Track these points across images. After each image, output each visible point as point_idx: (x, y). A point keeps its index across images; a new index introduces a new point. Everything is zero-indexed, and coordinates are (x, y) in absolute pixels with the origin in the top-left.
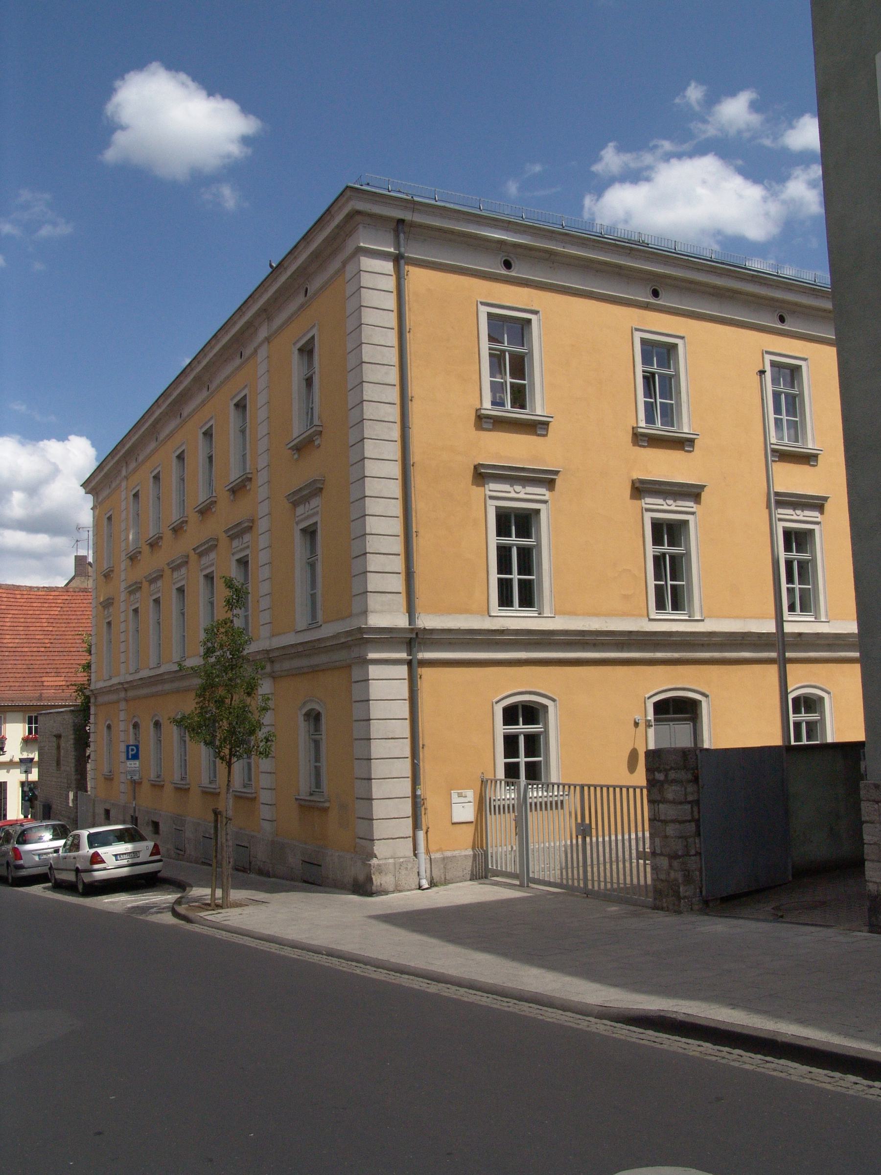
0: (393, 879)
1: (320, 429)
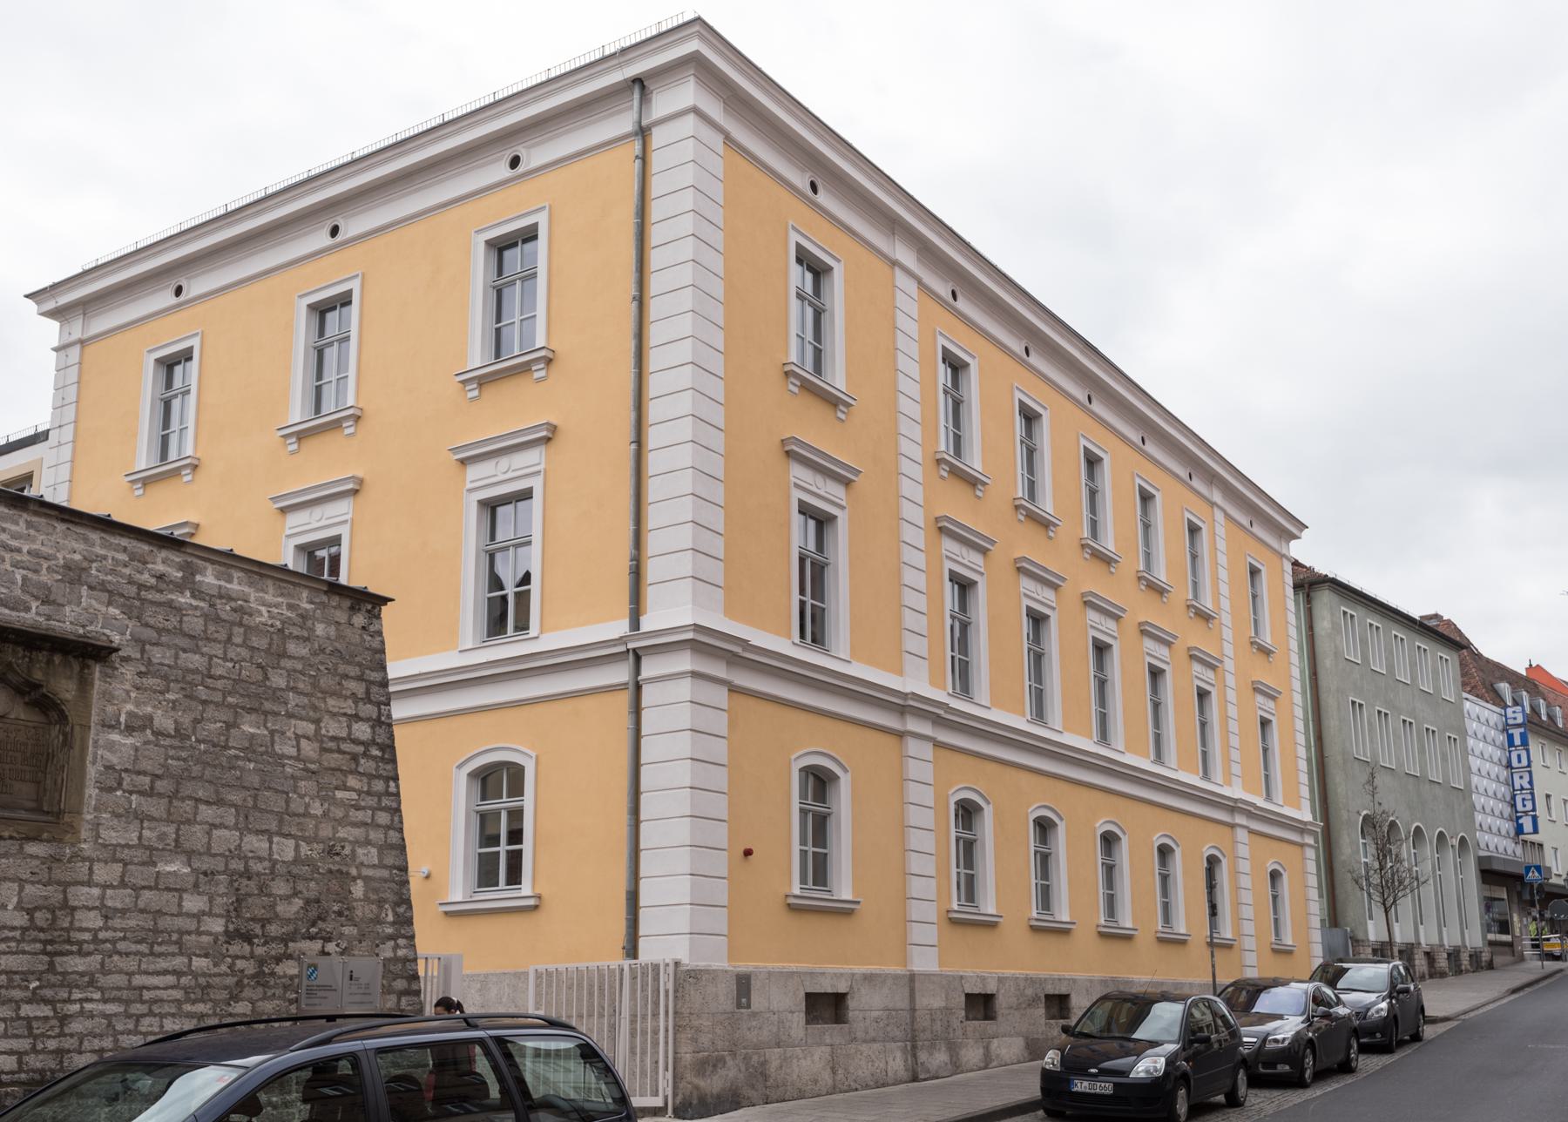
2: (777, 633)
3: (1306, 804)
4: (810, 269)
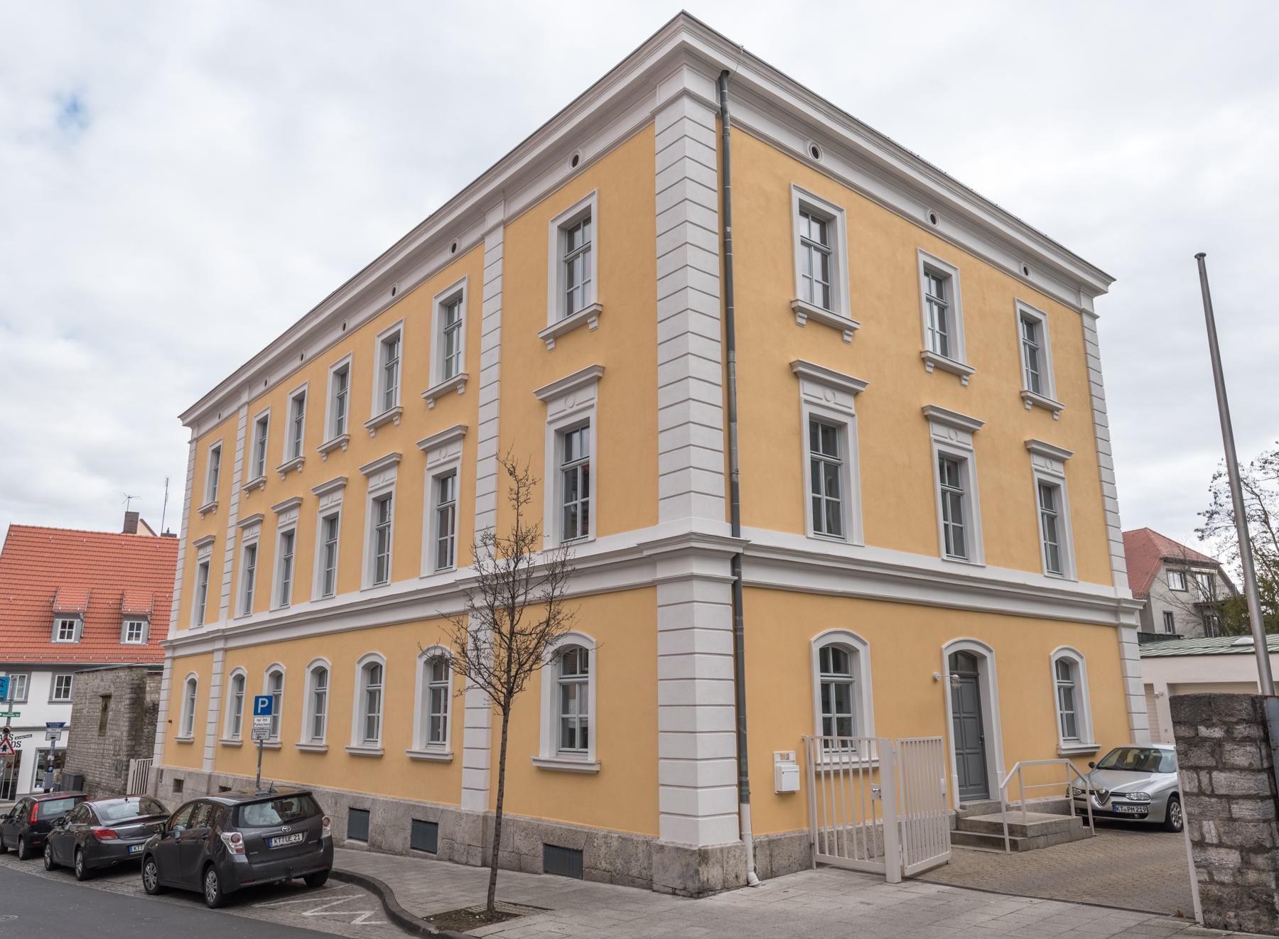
0: (720, 871)
1: (600, 309)
2: (930, 554)
3: (1122, 579)
4: (934, 278)
